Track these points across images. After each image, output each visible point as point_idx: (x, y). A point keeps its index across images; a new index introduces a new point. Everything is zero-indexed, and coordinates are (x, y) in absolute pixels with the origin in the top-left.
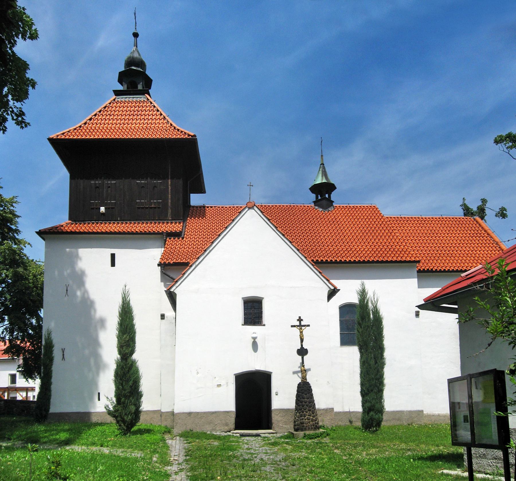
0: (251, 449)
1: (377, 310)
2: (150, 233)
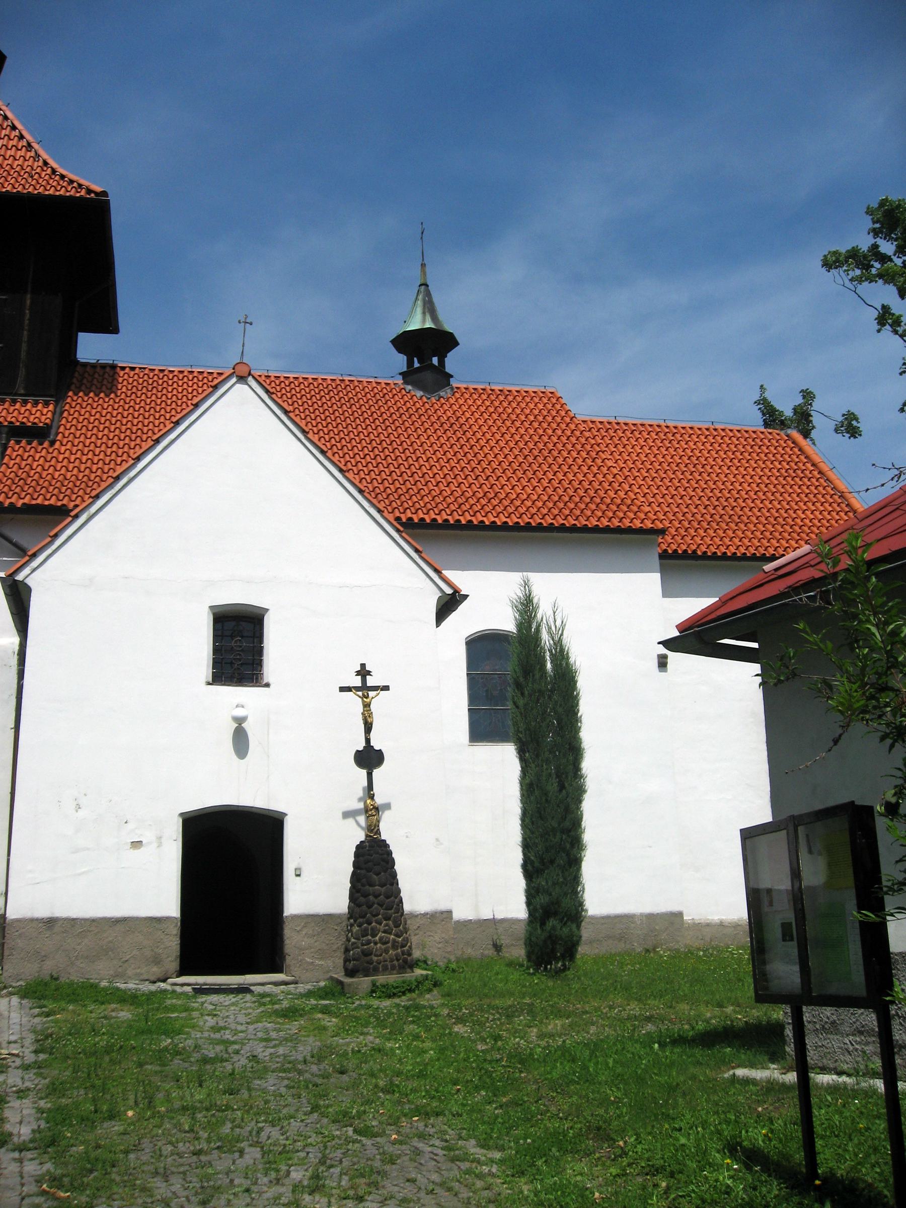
0: (225, 1028)
1: (562, 650)
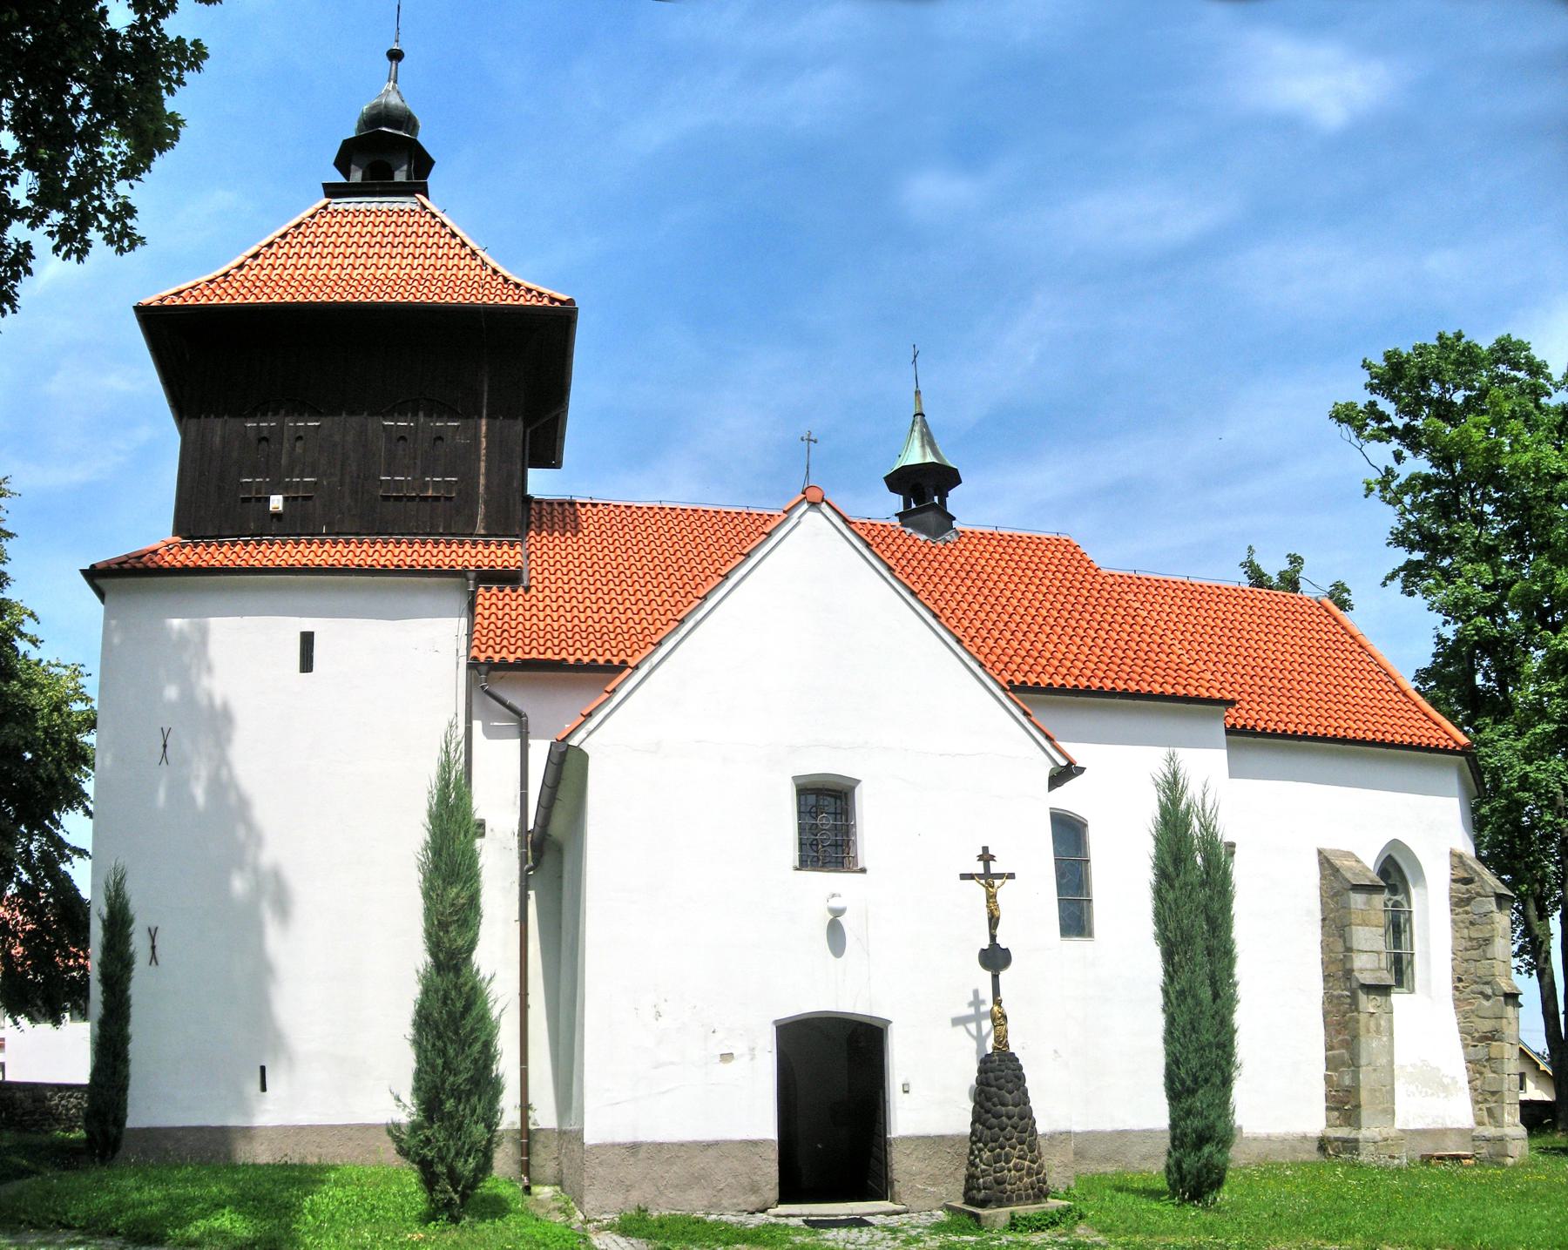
2: (425, 572)
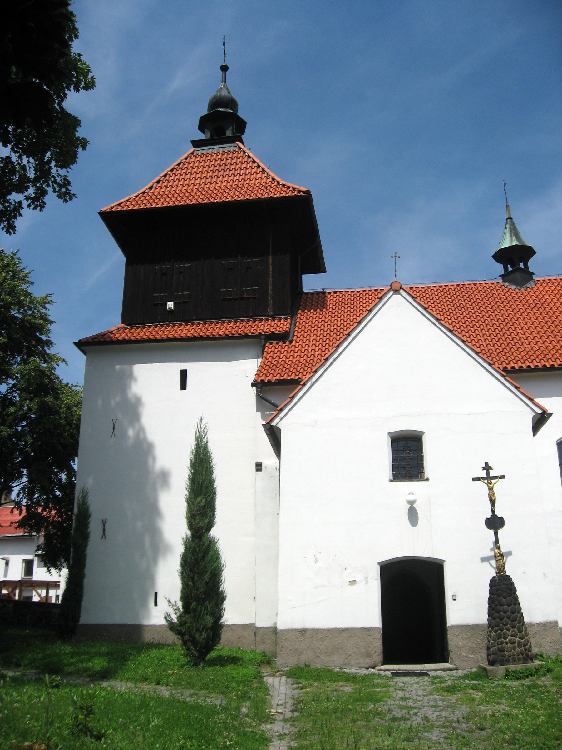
0: (410, 699)
2: (240, 337)
